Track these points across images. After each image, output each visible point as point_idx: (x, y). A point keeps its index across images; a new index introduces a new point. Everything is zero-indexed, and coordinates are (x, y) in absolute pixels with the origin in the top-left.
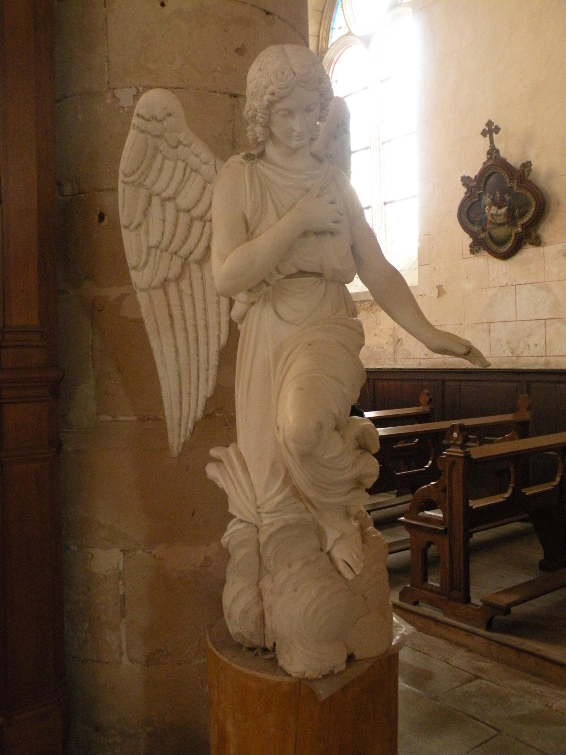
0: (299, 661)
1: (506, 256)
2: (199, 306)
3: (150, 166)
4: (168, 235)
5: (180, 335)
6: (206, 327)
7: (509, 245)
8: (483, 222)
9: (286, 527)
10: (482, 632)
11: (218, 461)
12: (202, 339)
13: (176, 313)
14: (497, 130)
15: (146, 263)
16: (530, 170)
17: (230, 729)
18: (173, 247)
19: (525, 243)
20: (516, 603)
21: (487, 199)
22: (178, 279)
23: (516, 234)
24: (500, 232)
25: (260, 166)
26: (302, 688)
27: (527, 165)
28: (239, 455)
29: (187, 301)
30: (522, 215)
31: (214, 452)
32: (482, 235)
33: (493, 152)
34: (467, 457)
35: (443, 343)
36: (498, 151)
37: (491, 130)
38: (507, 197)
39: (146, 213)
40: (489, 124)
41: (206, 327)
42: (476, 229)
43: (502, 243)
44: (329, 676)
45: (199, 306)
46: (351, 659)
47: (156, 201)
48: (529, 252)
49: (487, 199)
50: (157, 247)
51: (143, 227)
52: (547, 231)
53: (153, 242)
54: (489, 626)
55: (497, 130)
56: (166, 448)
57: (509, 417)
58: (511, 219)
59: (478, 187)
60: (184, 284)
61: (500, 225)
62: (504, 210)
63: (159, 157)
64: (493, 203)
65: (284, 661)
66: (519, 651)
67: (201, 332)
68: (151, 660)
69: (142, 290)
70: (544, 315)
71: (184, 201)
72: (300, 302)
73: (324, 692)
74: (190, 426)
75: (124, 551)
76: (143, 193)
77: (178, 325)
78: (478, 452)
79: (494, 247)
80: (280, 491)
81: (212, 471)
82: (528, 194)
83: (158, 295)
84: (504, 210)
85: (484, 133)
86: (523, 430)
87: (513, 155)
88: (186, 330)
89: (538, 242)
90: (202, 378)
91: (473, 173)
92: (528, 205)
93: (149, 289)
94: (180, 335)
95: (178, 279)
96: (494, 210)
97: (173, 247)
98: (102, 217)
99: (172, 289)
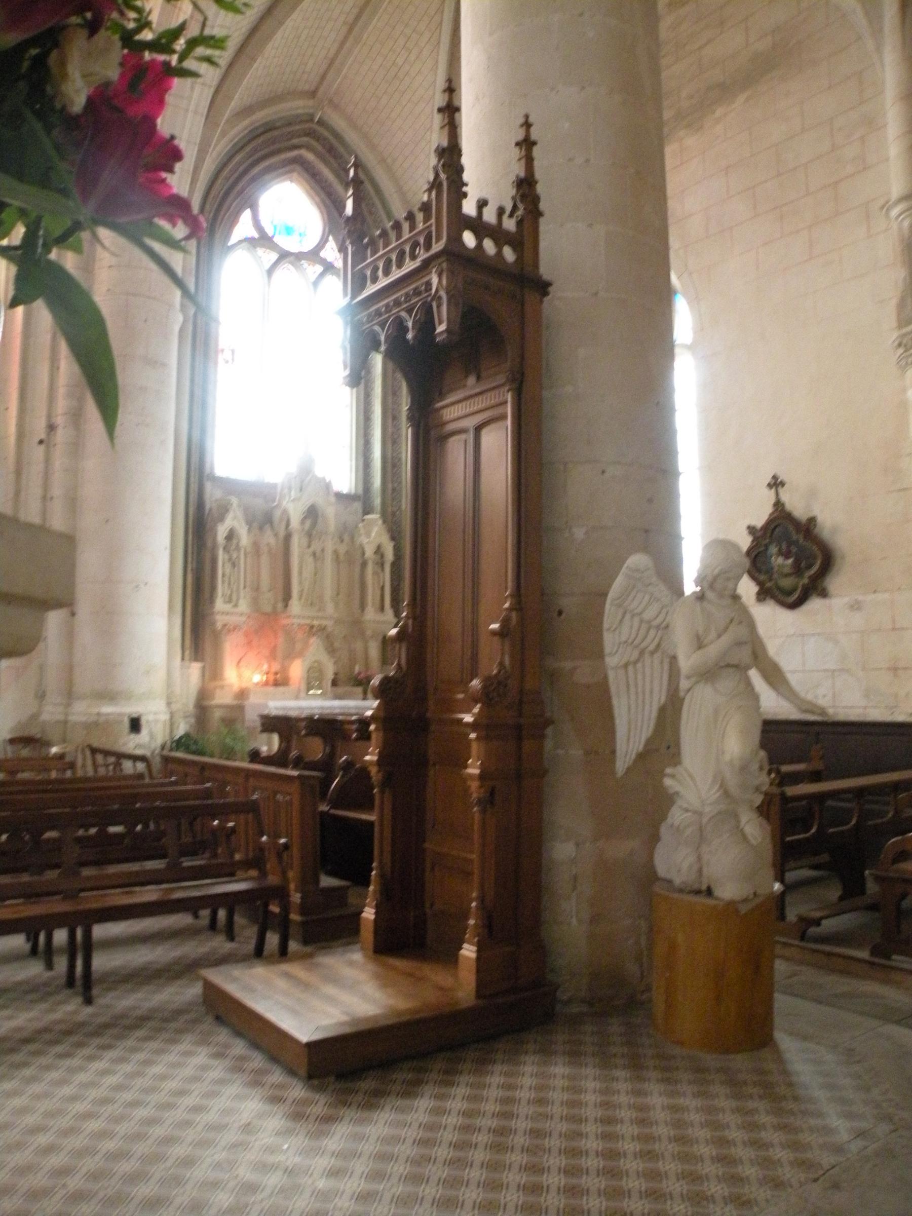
0: (728, 891)
1: (793, 606)
2: (648, 680)
3: (628, 596)
4: (633, 636)
5: (633, 697)
6: (651, 692)
7: (796, 596)
8: (769, 572)
9: (720, 813)
10: (796, 942)
11: (673, 776)
12: (647, 701)
13: (631, 683)
14: (782, 484)
15: (617, 651)
16: (815, 525)
17: (680, 938)
18: (636, 642)
19: (811, 595)
20: (826, 917)
21: (773, 549)
22: (636, 662)
23: (803, 585)
24: (787, 583)
25: (705, 603)
26: (731, 905)
27: (812, 520)
28: (686, 770)
29: (640, 677)
30: (809, 567)
31: (668, 770)
32: (768, 585)
33: (778, 505)
34: (783, 794)
35: (811, 708)
36: (783, 505)
37: (776, 483)
38: (794, 549)
39: (621, 621)
40: (775, 477)
41: (651, 692)
42: (762, 577)
43: (789, 593)
44: (745, 901)
45: (648, 680)
46: (755, 894)
47: (628, 617)
48: (815, 604)
49: (773, 549)
50: (626, 642)
51: (617, 632)
52: (834, 583)
53: (623, 639)
54: (803, 938)
55: (782, 484)
56: (613, 772)
57: (801, 767)
58: (798, 570)
59: (763, 536)
60: (639, 665)
61: (787, 575)
62: (790, 561)
63: (635, 590)
64: (780, 553)
65: (717, 892)
66: (829, 954)
67: (647, 696)
68: (594, 920)
69: (613, 668)
70: (831, 666)
71: (647, 615)
72: (728, 683)
73: (744, 909)
74: (634, 756)
75: (577, 845)
76: (621, 611)
77: (632, 690)
78: (792, 791)
79: (780, 597)
80: (718, 791)
81: (668, 782)
82: (815, 548)
83: (621, 672)
84: (790, 561)
85: (770, 486)
86: (816, 777)
87: (798, 507)
88: (637, 693)
89: (824, 594)
90: (645, 726)
91: (759, 522)
92: (815, 558)
93: (616, 668)
94: (633, 697)
95: (636, 662)
96: (780, 560)
97: (636, 642)
98: (560, 613)
99: (630, 668)
